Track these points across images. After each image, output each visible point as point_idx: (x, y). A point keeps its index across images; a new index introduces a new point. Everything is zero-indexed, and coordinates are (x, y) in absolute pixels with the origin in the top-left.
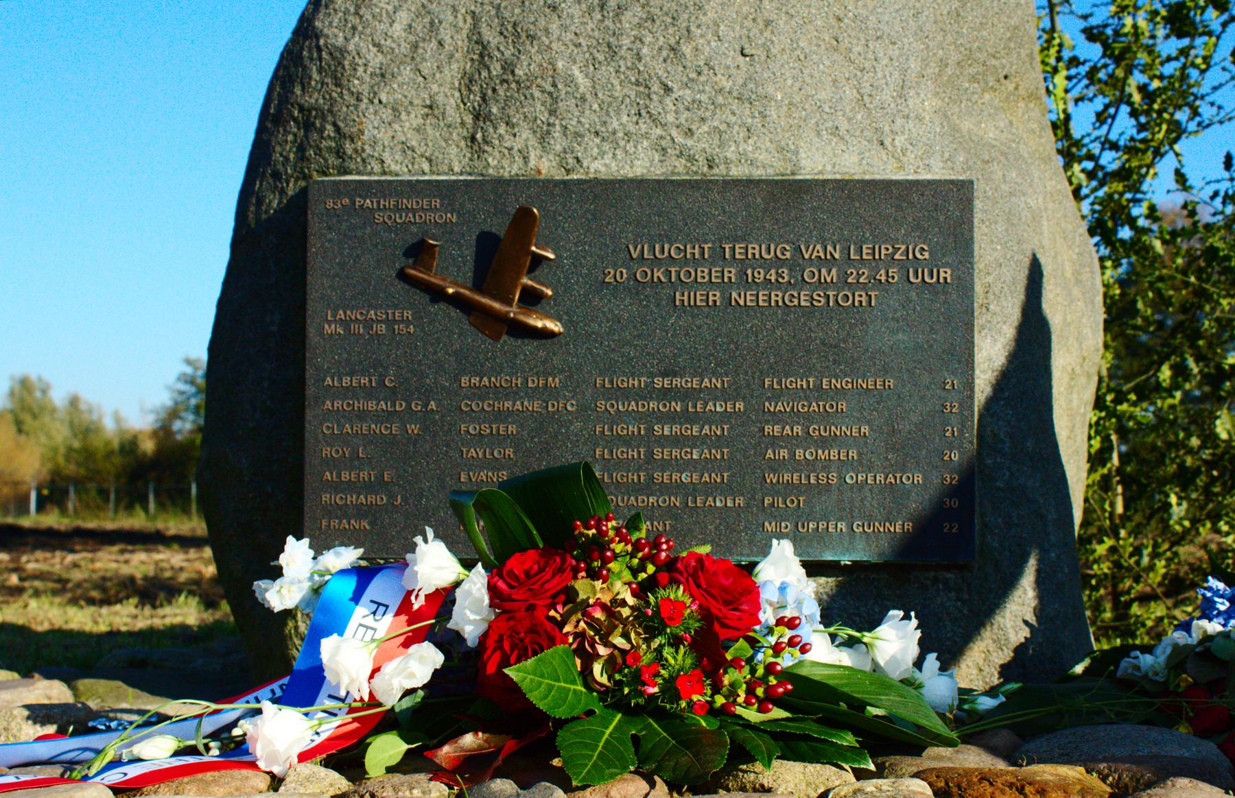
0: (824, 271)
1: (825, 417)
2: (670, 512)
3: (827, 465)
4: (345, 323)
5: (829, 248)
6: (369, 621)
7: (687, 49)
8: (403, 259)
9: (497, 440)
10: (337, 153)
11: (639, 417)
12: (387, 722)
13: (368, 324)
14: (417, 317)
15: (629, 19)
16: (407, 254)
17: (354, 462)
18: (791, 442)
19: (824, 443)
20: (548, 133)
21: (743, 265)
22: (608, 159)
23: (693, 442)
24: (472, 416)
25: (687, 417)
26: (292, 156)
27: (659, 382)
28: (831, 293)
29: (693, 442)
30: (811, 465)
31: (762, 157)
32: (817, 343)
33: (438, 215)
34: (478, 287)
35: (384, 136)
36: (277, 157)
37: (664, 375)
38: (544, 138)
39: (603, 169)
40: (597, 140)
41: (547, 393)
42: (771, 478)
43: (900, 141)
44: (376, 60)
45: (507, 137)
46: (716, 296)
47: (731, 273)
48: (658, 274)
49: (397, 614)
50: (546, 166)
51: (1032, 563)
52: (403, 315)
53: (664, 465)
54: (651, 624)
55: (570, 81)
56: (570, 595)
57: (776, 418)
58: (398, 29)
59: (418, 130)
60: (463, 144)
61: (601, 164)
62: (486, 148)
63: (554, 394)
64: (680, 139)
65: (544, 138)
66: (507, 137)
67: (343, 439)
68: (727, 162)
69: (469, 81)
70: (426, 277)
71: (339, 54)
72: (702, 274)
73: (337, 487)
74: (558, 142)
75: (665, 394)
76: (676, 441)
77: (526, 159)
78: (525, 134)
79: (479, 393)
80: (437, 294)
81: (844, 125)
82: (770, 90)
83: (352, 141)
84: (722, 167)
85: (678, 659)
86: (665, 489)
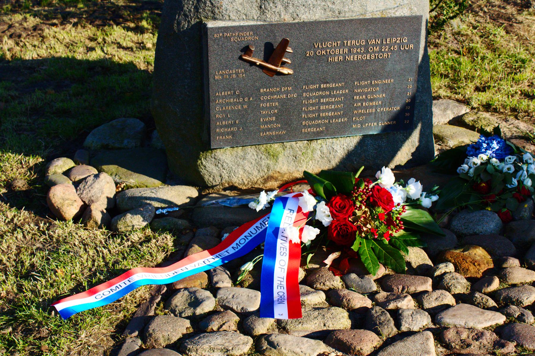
0: (375, 48)
1: (372, 93)
2: (325, 124)
3: (372, 107)
4: (222, 75)
5: (377, 40)
6: (289, 215)
8: (240, 52)
9: (271, 108)
10: (212, 12)
11: (316, 97)
13: (230, 75)
14: (246, 71)
17: (226, 118)
18: (361, 101)
19: (371, 100)
20: (288, 6)
21: (352, 47)
22: (307, 14)
23: (332, 103)
25: (330, 96)
26: (192, 10)
27: (322, 86)
28: (377, 55)
29: (332, 103)
30: (366, 108)
31: (356, 9)
33: (248, 37)
34: (266, 60)
36: (185, 8)
37: (324, 83)
38: (286, 8)
39: (306, 18)
40: (304, 8)
42: (355, 112)
45: (273, 7)
46: (341, 58)
47: (346, 50)
48: (323, 52)
49: (297, 212)
50: (287, 18)
51: (420, 125)
52: (239, 72)
53: (324, 111)
59: (241, 4)
60: (257, 9)
61: (306, 16)
62: (266, 11)
64: (330, 6)
65: (286, 8)
66: (273, 7)
68: (345, 12)
70: (249, 59)
74: (291, 9)
75: (325, 89)
76: (328, 103)
77: (280, 15)
78: (279, 6)
79: (266, 94)
80: (253, 64)
83: (218, 8)
84: (343, 14)
86: (324, 118)
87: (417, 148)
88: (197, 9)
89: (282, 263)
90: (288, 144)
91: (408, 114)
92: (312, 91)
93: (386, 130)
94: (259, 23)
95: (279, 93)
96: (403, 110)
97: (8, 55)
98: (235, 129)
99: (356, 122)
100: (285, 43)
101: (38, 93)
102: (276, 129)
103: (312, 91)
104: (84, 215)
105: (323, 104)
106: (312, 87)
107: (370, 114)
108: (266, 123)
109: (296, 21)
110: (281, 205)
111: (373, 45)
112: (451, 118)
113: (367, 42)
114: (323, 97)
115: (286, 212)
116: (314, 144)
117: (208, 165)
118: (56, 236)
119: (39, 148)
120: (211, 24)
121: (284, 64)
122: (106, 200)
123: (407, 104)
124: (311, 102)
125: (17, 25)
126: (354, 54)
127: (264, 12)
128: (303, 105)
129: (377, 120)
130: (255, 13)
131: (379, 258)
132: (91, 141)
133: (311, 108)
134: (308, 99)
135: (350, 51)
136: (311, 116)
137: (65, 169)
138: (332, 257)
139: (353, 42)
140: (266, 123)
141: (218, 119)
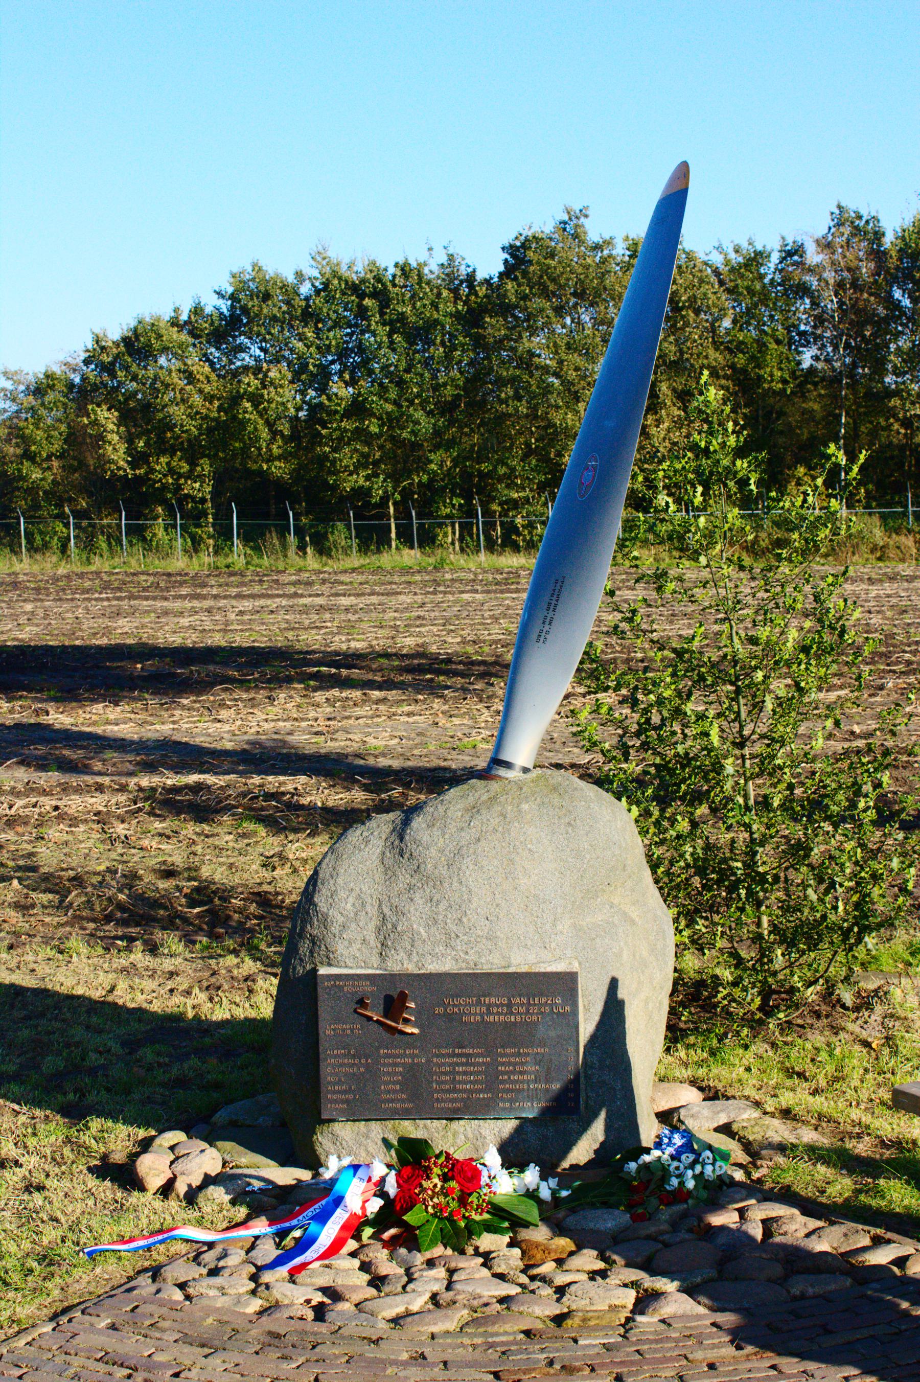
1: (522, 1064)
2: (462, 1100)
3: (522, 1082)
4: (334, 1030)
7: (465, 920)
9: (396, 1074)
11: (450, 1065)
12: (368, 1223)
13: (343, 1030)
15: (442, 907)
16: (357, 1003)
18: (507, 1073)
19: (521, 1073)
21: (489, 1006)
23: (471, 1073)
24: (384, 1065)
27: (457, 1051)
29: (471, 1073)
30: (516, 1082)
31: (496, 961)
32: (516, 1036)
33: (368, 988)
34: (386, 1016)
35: (346, 953)
41: (413, 1056)
42: (502, 1086)
43: (553, 945)
44: (341, 919)
46: (478, 1018)
47: (484, 1009)
48: (456, 1010)
50: (411, 968)
51: (603, 1115)
52: (354, 1027)
53: (460, 1082)
54: (446, 1193)
55: (419, 933)
56: (421, 1185)
57: (503, 1064)
58: (349, 906)
61: (432, 967)
63: (417, 1056)
67: (335, 1074)
69: (379, 930)
71: (325, 917)
72: (473, 1010)
73: (334, 1092)
74: (415, 958)
75: (459, 1055)
76: (465, 1073)
78: (402, 954)
79: (388, 1056)
80: (370, 1019)
81: (529, 943)
82: (499, 934)
85: (454, 1205)
86: (460, 1091)
87: (602, 1144)
88: (312, 952)
89: (331, 1231)
90: (421, 1123)
91: (572, 1095)
92: (444, 1056)
93: (544, 1112)
94: (378, 972)
95: (404, 1056)
96: (565, 1090)
97: (190, 1014)
98: (351, 1096)
99: (502, 1099)
100: (403, 997)
101: (194, 1061)
102: (403, 1101)
103: (444, 1056)
104: (167, 1190)
105: (459, 1073)
106: (444, 1051)
107: (519, 1091)
108: (389, 1092)
109: (422, 972)
110: (351, 1171)
111: (518, 1005)
112: (721, 1123)
113: (509, 1000)
114: (458, 1064)
115: (356, 1180)
116: (455, 1125)
117: (324, 1142)
118: (128, 1205)
119: (158, 1121)
120: (323, 971)
121: (406, 1021)
122: (202, 1176)
123: (571, 1082)
124: (443, 1069)
125: (223, 971)
126: (515, 1014)
127: (384, 960)
128: (432, 1073)
129: (530, 1099)
130: (375, 960)
131: (443, 1238)
132: (221, 1117)
133: (443, 1078)
134: (440, 1065)
135: (488, 1009)
136: (443, 1087)
137: (172, 1143)
138: (393, 1231)
139: (493, 1000)
140: (389, 1092)
141: (330, 1083)
